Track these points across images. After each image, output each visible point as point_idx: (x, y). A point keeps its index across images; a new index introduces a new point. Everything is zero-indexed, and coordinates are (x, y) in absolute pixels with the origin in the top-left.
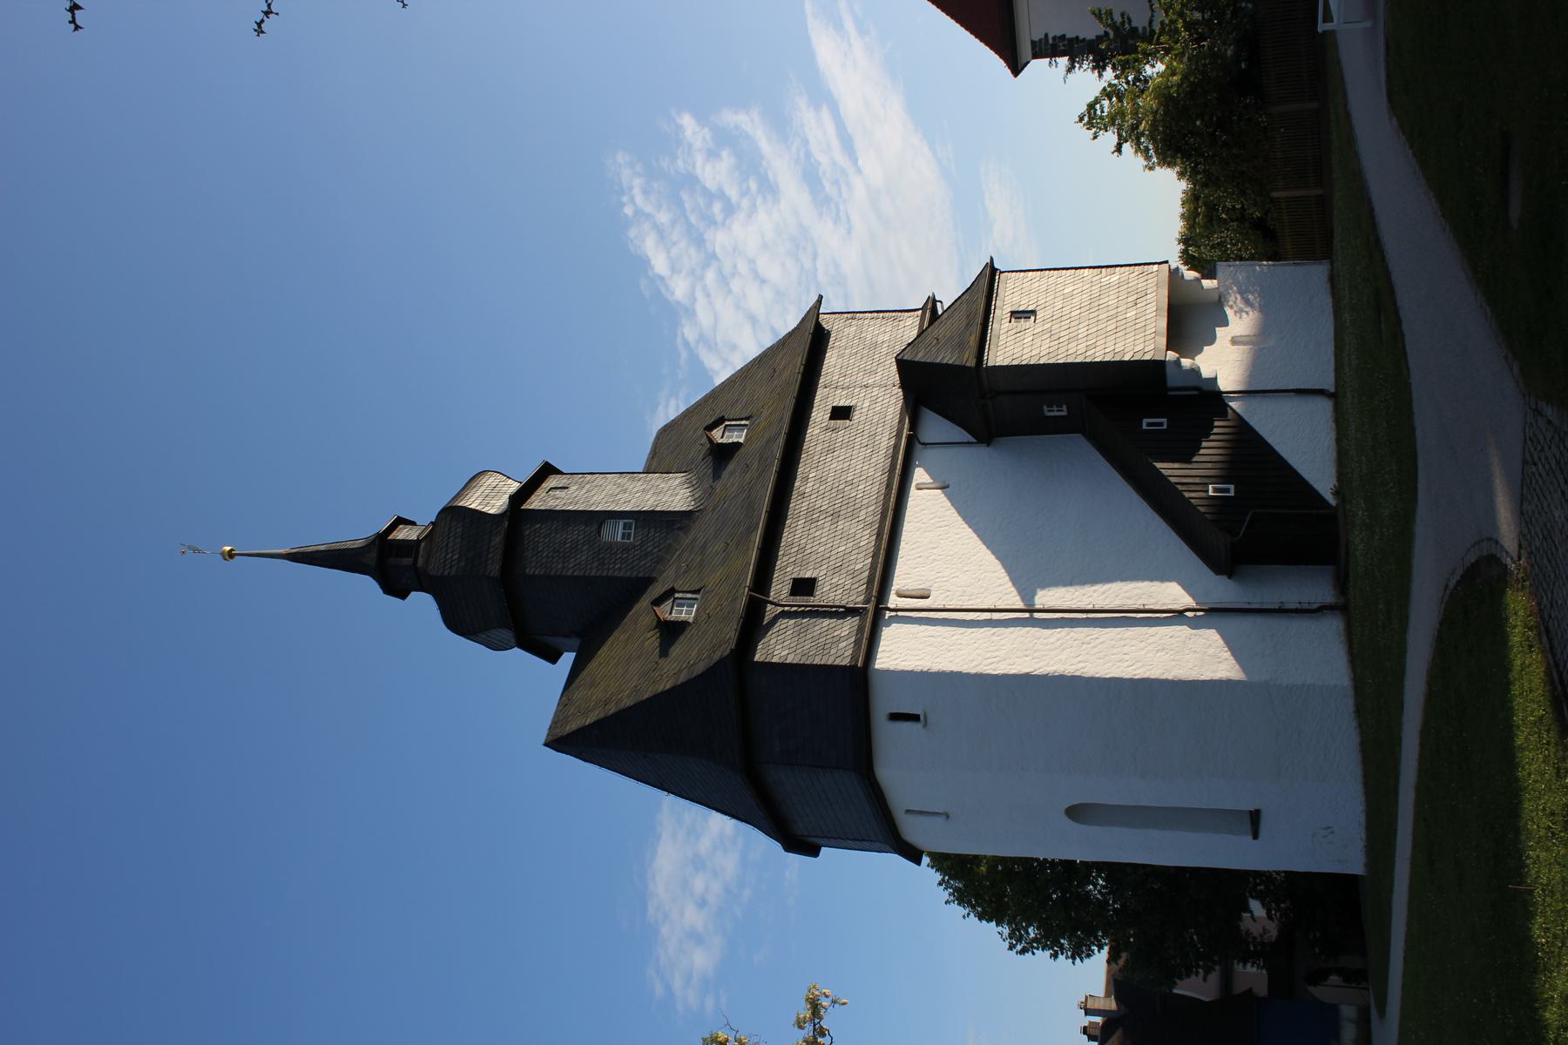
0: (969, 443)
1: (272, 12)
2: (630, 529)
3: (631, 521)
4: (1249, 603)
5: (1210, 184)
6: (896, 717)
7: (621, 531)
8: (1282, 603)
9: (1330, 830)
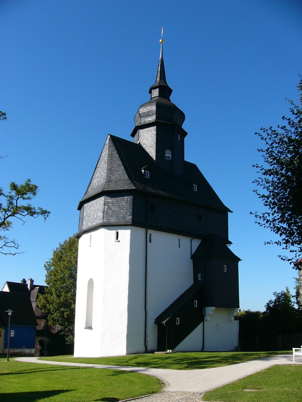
1: (33, 216)
2: (169, 158)
5: (244, 361)
6: (117, 233)
7: (168, 156)
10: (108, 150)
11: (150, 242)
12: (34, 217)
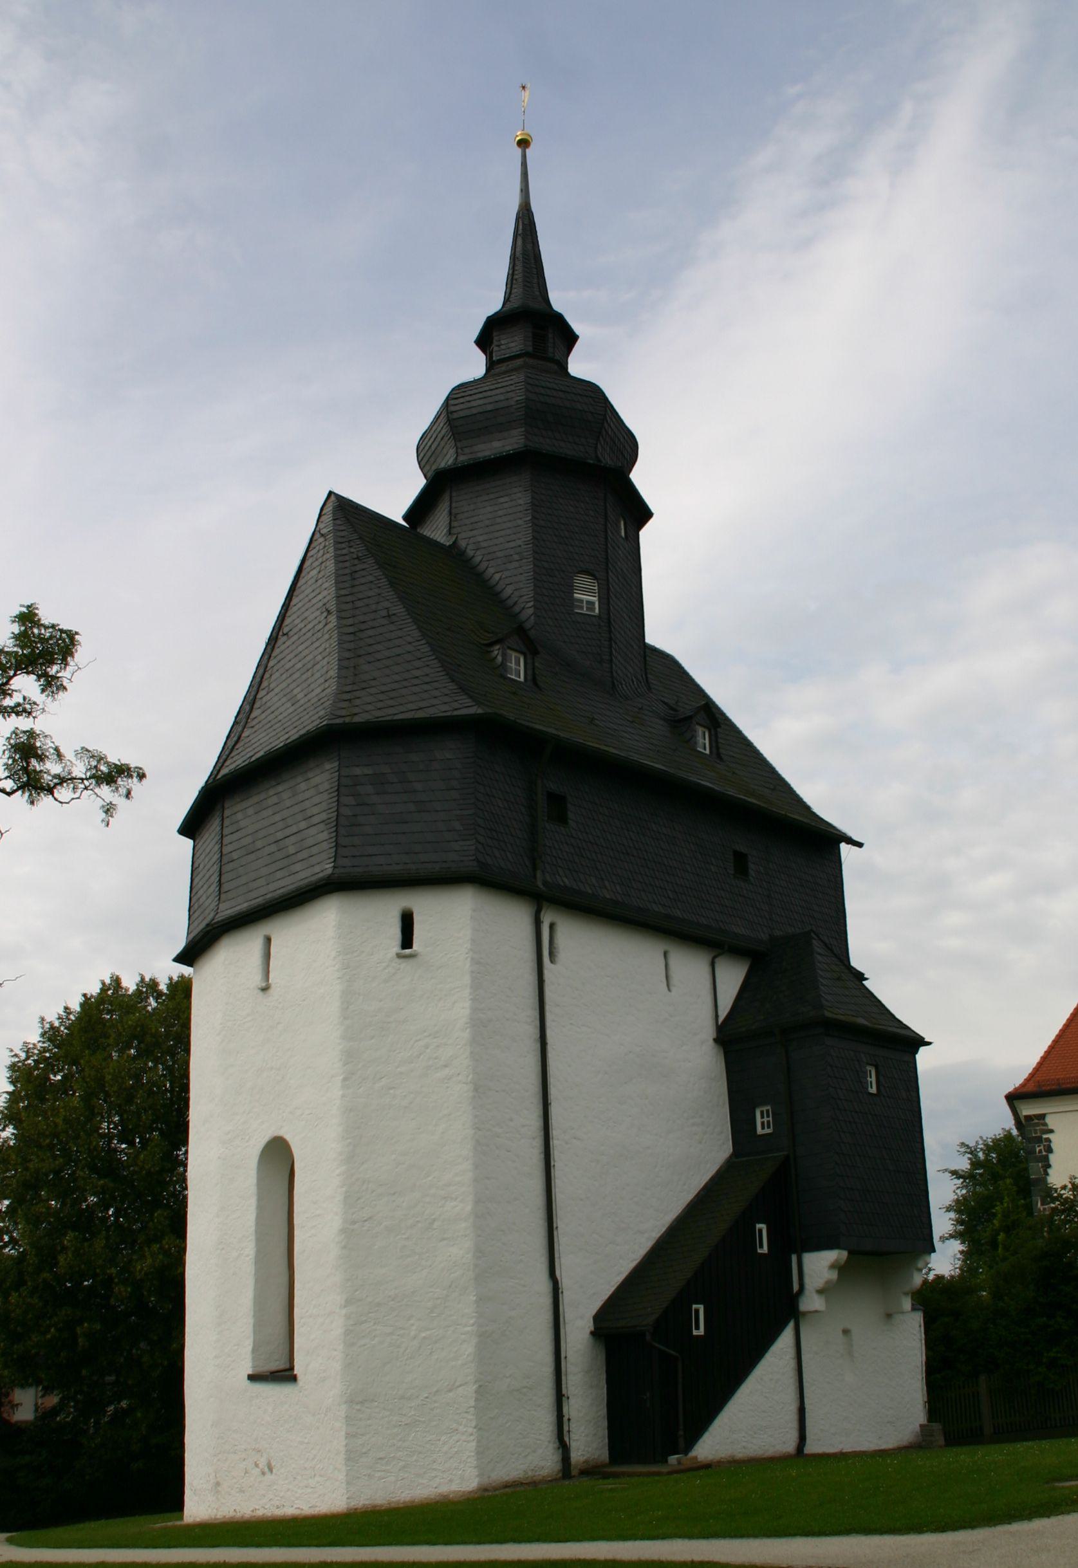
0: (717, 1016)
1: (52, 794)
3: (597, 611)
4: (566, 1357)
6: (407, 922)
8: (568, 1398)
9: (266, 1470)
10: (336, 556)
11: (552, 960)
12: (56, 799)
